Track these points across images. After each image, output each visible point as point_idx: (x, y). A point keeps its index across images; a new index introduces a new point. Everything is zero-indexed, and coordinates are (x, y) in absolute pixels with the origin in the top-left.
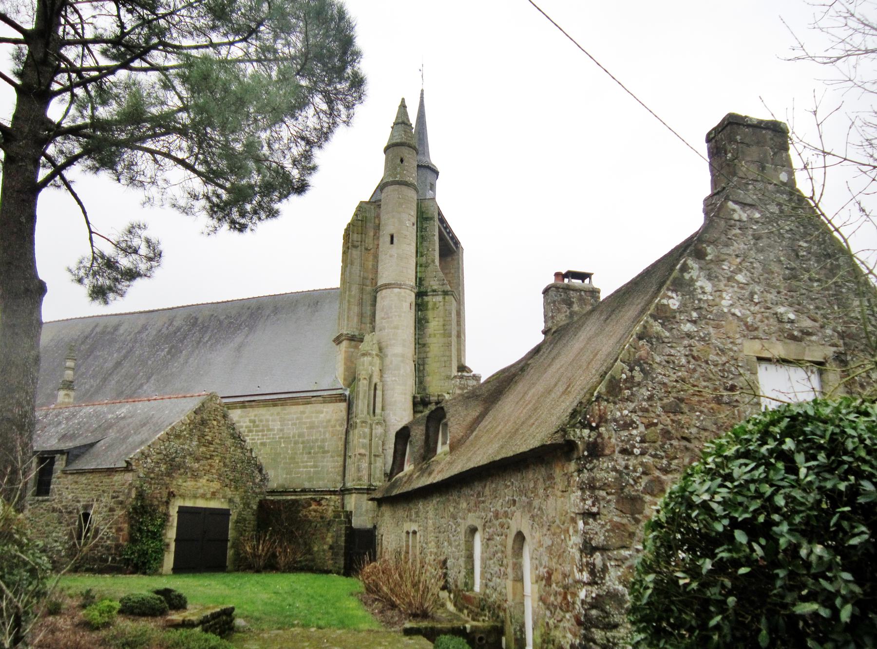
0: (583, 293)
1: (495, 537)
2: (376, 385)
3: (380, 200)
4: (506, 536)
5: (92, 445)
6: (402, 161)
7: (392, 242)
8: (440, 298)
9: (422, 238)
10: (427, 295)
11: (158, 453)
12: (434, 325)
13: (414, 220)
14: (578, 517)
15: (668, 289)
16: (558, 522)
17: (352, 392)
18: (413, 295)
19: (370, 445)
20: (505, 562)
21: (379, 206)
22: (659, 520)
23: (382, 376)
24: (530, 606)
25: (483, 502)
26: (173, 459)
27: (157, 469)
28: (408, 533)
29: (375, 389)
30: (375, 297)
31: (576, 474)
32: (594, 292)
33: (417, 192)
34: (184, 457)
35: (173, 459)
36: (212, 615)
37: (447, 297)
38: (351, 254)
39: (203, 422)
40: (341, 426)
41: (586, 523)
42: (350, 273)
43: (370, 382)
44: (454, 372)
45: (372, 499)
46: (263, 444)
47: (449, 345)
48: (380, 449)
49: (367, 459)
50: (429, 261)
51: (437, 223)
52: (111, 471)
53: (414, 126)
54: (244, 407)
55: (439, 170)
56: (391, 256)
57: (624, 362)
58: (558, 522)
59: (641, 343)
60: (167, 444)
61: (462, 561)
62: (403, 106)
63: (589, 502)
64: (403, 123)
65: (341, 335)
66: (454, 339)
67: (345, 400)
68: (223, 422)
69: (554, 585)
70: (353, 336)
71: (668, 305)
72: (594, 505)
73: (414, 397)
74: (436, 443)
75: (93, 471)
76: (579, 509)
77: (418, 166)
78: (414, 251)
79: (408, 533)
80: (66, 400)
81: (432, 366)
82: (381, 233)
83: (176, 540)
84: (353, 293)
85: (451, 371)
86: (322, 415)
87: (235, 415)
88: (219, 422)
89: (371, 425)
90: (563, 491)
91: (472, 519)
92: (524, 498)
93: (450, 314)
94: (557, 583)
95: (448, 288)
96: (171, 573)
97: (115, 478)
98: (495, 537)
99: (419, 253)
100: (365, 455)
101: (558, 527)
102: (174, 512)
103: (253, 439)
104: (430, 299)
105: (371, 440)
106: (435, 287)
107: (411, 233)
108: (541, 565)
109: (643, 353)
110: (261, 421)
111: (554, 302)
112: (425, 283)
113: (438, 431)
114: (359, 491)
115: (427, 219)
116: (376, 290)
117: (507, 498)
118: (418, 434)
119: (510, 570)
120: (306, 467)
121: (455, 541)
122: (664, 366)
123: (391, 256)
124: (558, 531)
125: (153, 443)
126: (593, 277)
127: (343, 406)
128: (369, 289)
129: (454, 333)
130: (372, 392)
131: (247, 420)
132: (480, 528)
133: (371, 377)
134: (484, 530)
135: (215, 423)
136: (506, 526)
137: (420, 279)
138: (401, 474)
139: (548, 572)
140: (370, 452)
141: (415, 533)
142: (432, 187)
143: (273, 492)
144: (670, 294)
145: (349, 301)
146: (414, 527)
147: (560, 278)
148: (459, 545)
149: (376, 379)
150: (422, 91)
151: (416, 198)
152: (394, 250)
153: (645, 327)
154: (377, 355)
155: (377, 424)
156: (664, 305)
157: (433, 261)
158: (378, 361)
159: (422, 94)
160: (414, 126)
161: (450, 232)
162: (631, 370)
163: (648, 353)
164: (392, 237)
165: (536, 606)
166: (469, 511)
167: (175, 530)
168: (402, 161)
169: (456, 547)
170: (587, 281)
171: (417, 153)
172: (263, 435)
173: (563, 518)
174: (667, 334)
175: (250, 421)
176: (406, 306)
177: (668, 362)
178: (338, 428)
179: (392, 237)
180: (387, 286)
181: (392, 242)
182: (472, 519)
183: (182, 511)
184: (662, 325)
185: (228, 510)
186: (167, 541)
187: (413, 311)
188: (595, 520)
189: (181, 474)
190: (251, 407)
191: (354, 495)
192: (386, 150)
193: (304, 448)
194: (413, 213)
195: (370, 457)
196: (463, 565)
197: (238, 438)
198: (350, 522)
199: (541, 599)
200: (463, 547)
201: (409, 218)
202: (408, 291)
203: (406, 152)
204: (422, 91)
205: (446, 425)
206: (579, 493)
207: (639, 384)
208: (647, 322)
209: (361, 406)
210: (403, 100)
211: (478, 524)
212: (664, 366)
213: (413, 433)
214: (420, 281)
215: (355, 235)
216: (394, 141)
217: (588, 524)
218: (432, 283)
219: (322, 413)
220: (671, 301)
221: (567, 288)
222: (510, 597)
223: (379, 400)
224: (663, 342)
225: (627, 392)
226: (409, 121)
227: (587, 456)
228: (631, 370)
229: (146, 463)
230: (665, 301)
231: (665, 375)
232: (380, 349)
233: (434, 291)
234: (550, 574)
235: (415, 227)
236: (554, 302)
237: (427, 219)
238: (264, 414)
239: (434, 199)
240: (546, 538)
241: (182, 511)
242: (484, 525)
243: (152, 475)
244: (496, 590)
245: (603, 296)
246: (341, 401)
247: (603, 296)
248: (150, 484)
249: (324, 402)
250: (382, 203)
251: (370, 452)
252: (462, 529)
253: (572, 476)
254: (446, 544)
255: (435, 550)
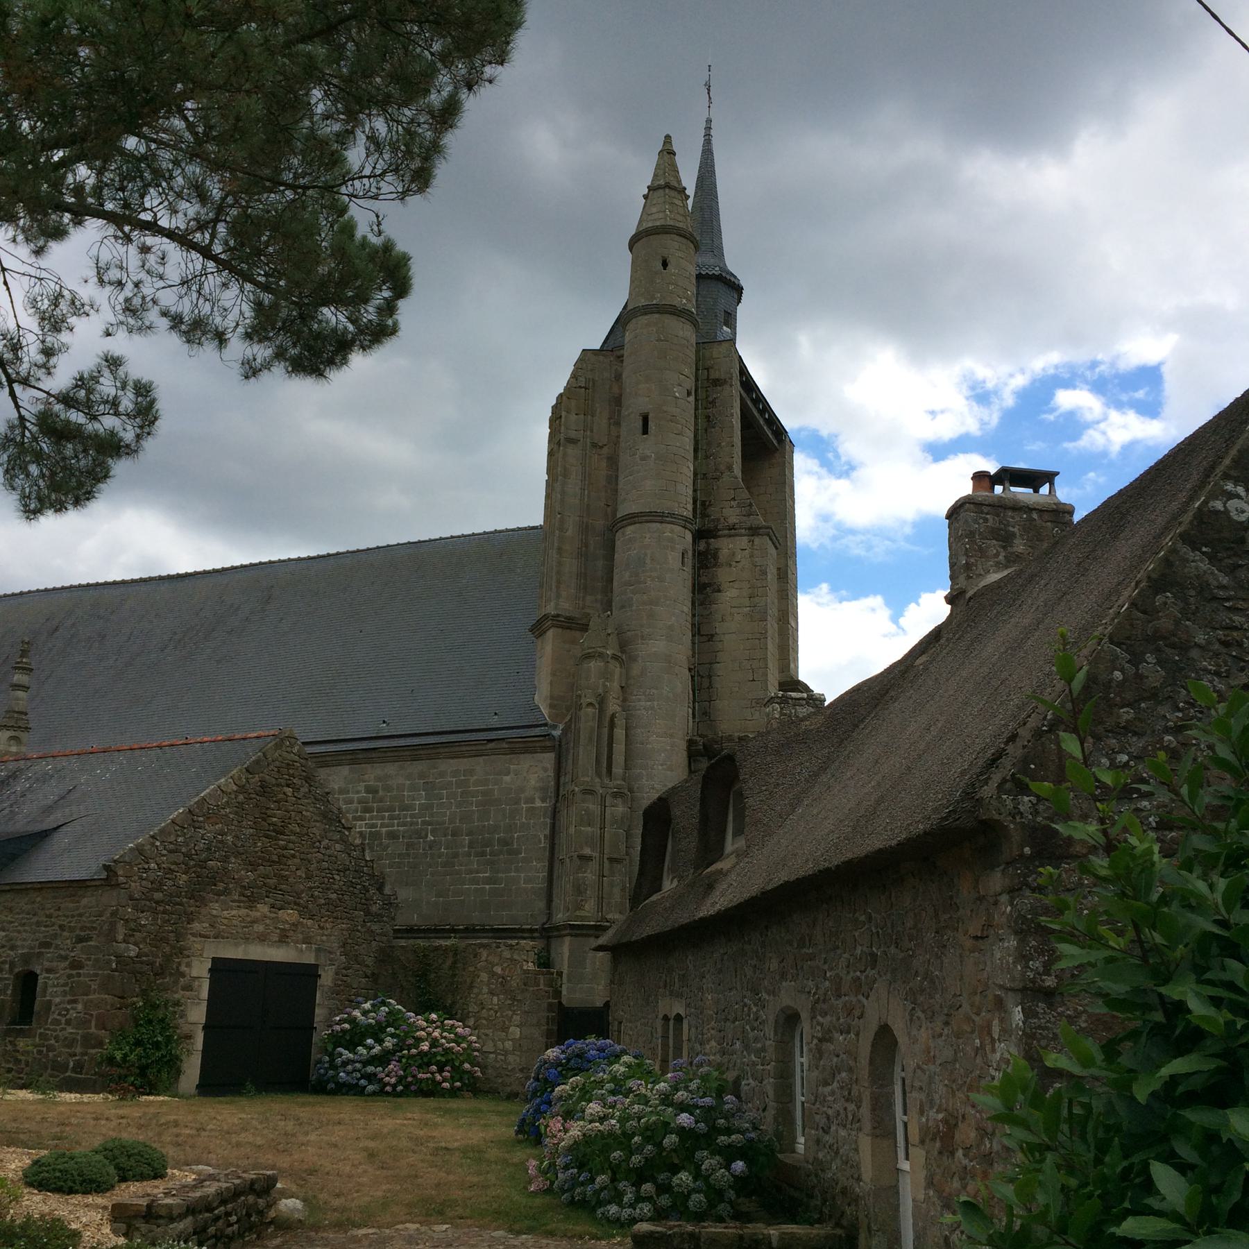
0: (1035, 516)
1: (836, 1035)
2: (613, 716)
3: (622, 347)
4: (857, 1035)
5: (45, 835)
6: (665, 264)
7: (645, 431)
8: (743, 542)
9: (706, 421)
10: (715, 537)
11: (170, 851)
12: (730, 597)
13: (690, 384)
14: (1010, 999)
15: (1226, 476)
16: (966, 1007)
17: (565, 731)
18: (689, 536)
19: (602, 838)
20: (855, 1092)
21: (620, 358)
22: (1229, 920)
23: (625, 700)
24: (910, 1191)
25: (812, 957)
26: (202, 864)
27: (170, 883)
28: (666, 1018)
29: (612, 725)
30: (613, 542)
31: (1004, 898)
32: (1061, 512)
33: (695, 324)
34: (225, 859)
35: (202, 864)
36: (219, 1193)
37: (757, 540)
38: (565, 455)
39: (264, 788)
40: (543, 800)
41: (1028, 1014)
42: (563, 493)
43: (601, 711)
44: (773, 690)
45: (600, 948)
46: (393, 836)
47: (763, 635)
48: (623, 847)
49: (594, 866)
50: (722, 467)
51: (736, 390)
52: (77, 887)
53: (691, 191)
54: (353, 762)
55: (742, 283)
56: (644, 458)
57: (1119, 645)
58: (966, 1007)
59: (1159, 599)
60: (190, 832)
61: (769, 1085)
62: (668, 151)
63: (1036, 964)
64: (667, 186)
65: (546, 617)
66: (772, 627)
67: (550, 749)
68: (305, 790)
69: (960, 1153)
70: (570, 619)
71: (1227, 512)
72: (1047, 972)
73: (691, 743)
74: (723, 832)
75: (42, 887)
76: (1013, 979)
77: (700, 277)
78: (690, 447)
79: (666, 1018)
80: (14, 749)
81: (728, 676)
82: (624, 413)
83: (206, 1028)
84: (569, 533)
85: (766, 689)
86: (507, 778)
87: (336, 779)
88: (296, 789)
89: (603, 798)
90: (976, 938)
91: (787, 996)
92: (893, 950)
93: (764, 573)
94: (967, 1150)
95: (760, 520)
96: (193, 1091)
97: (85, 901)
98: (836, 1035)
99: (700, 449)
100: (589, 858)
101: (969, 1019)
102: (200, 969)
103: (373, 826)
104: (726, 546)
105: (602, 828)
106: (733, 520)
107: (685, 409)
108: (932, 1102)
109: (1165, 623)
110: (388, 788)
111: (971, 535)
112: (714, 511)
113: (727, 808)
114: (579, 931)
115: (717, 382)
116: (615, 525)
117: (858, 951)
118: (686, 816)
119: (865, 1111)
120: (475, 881)
121: (756, 1040)
122: (1217, 655)
123: (644, 458)
124: (967, 1028)
125: (162, 831)
126: (1057, 479)
127: (548, 759)
128: (600, 524)
129: (773, 611)
130: (605, 731)
131: (361, 787)
132: (804, 1015)
133: (602, 701)
134: (813, 1018)
135: (289, 791)
136: (857, 1013)
137: (703, 503)
138: (654, 898)
139: (945, 1121)
140: (602, 853)
141: (679, 1018)
142: (730, 319)
143: (411, 931)
144: (1230, 487)
145: (560, 550)
146: (679, 1008)
147: (987, 483)
148: (763, 1049)
149: (613, 706)
150: (709, 121)
151: (693, 341)
152: (647, 446)
153: (1167, 561)
154: (615, 657)
155: (615, 795)
156: (1217, 512)
157: (730, 468)
158: (618, 670)
159: (708, 128)
160: (691, 191)
161: (766, 409)
162: (1136, 660)
163: (1177, 623)
164: (645, 420)
165: (921, 1197)
166: (783, 976)
167: (203, 1007)
168: (665, 264)
169: (758, 1052)
170: (1045, 489)
171: (697, 248)
172: (391, 818)
173: (977, 998)
174: (1225, 580)
175: (369, 790)
176: (673, 559)
177: (1226, 644)
178: (538, 804)
179: (645, 420)
180: (633, 518)
181: (645, 431)
182: (787, 996)
183: (220, 968)
184: (1212, 558)
185: (316, 966)
186: (185, 1029)
187: (688, 569)
188: (1051, 1006)
189: (219, 894)
190: (370, 761)
191: (567, 940)
192: (632, 244)
193: (471, 845)
194: (689, 371)
195: (601, 865)
196: (771, 1093)
197: (333, 819)
198: (558, 994)
199: (930, 1183)
200: (770, 1054)
201: (681, 380)
202: (679, 528)
203: (674, 248)
204: (709, 121)
205: (740, 795)
206: (1012, 943)
207: (1153, 695)
208: (1173, 551)
209: (584, 757)
210: (668, 138)
211: (803, 1006)
212: (1217, 655)
213: (676, 812)
214: (702, 506)
215: (573, 417)
216: (645, 225)
217: (1036, 1015)
218: (727, 512)
219: (508, 774)
220: (1233, 504)
221: (1001, 506)
222: (867, 1173)
223: (619, 748)
224: (1215, 598)
225: (1126, 714)
226: (679, 182)
227: (1031, 858)
228: (1136, 660)
229: (146, 870)
230: (1218, 505)
231: (1217, 674)
232: (623, 645)
233: (732, 528)
234: (951, 1123)
235: (692, 398)
236: (971, 535)
237: (717, 382)
238: (397, 775)
239: (733, 341)
240: (940, 1042)
241: (220, 968)
242: (813, 1009)
243: (158, 896)
244: (837, 1153)
245: (1077, 517)
246: (545, 749)
247: (1077, 517)
248: (155, 912)
249: (513, 752)
250: (626, 353)
251: (602, 853)
252: (770, 1015)
253: (996, 903)
254: (738, 1045)
255: (718, 1058)
